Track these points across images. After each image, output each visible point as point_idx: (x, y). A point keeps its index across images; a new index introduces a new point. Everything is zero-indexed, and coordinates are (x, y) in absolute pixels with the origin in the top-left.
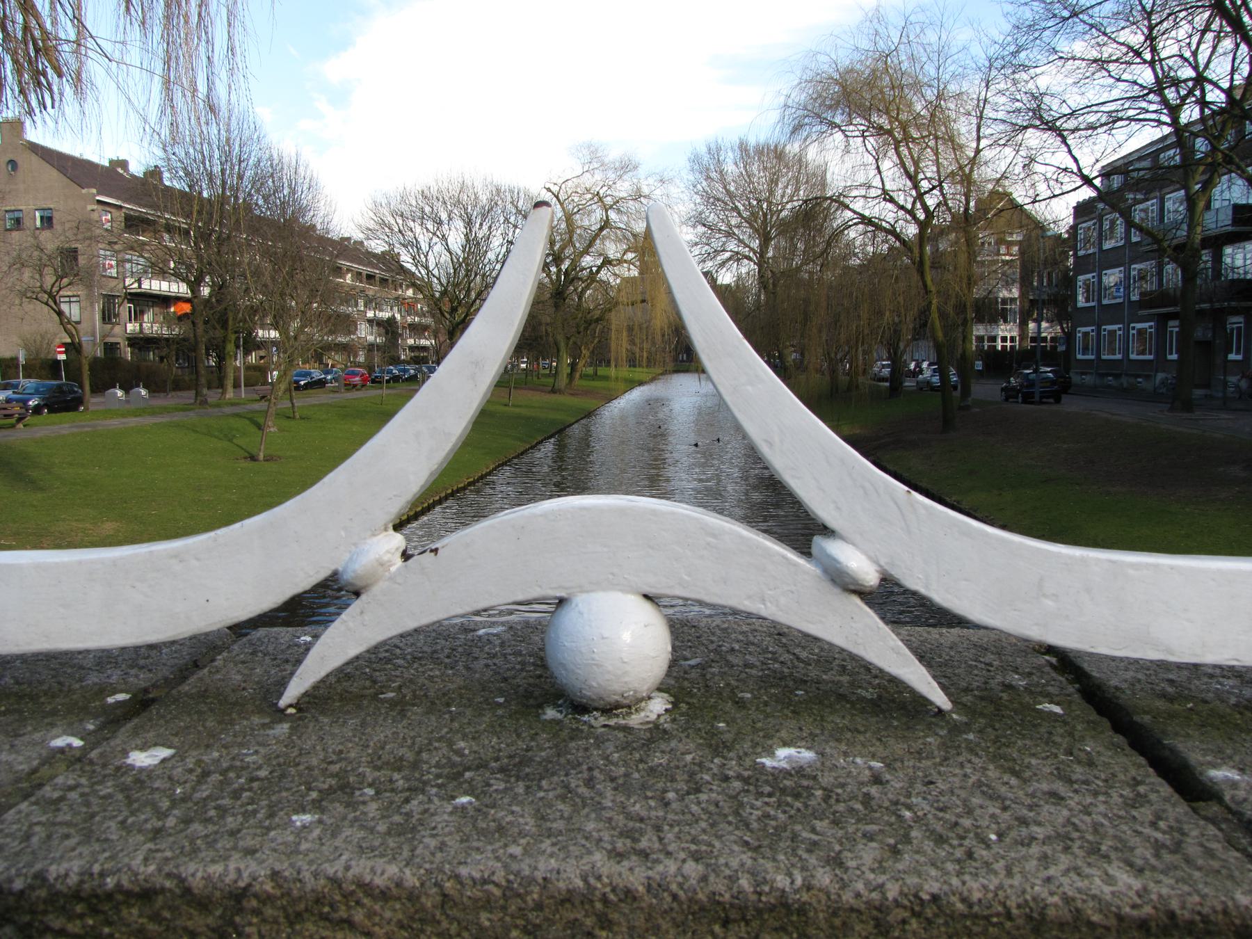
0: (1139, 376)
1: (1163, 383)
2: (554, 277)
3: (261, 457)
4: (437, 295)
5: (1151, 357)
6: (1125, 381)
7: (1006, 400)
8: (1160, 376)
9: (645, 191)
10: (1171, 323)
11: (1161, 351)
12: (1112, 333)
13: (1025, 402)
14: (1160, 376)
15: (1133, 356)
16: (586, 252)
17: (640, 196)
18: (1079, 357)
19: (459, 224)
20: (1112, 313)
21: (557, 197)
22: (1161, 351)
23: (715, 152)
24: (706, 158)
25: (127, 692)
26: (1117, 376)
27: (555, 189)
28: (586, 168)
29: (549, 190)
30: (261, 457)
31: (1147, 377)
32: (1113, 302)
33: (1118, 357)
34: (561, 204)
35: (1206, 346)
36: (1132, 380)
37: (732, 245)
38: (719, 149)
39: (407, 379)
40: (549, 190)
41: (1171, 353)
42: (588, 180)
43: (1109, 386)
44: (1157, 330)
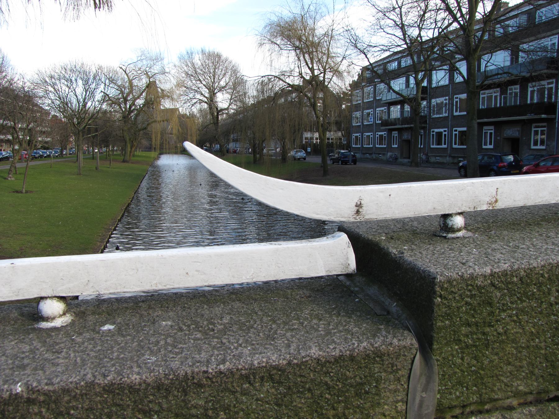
0: (380, 154)
1: (391, 157)
2: (124, 110)
3: (24, 191)
4: (423, 73)
5: (385, 146)
6: (374, 156)
7: (333, 163)
8: (389, 154)
9: (167, 70)
10: (393, 132)
11: (389, 144)
12: (368, 136)
13: (342, 164)
14: (389, 154)
15: (377, 146)
16: (138, 98)
17: (165, 73)
18: (354, 146)
19: (80, 82)
20: (369, 128)
21: (125, 72)
22: (389, 144)
23: (190, 54)
24: (186, 57)
25: (41, 329)
26: (370, 154)
27: (124, 68)
28: (139, 59)
29: (121, 68)
30: (24, 191)
31: (384, 154)
32: (368, 123)
33: (371, 146)
34: (127, 75)
35: (408, 142)
36: (377, 155)
37: (198, 96)
38: (192, 54)
39: (45, 157)
40: (121, 68)
41: (394, 145)
42: (139, 65)
43: (367, 158)
44: (388, 135)
